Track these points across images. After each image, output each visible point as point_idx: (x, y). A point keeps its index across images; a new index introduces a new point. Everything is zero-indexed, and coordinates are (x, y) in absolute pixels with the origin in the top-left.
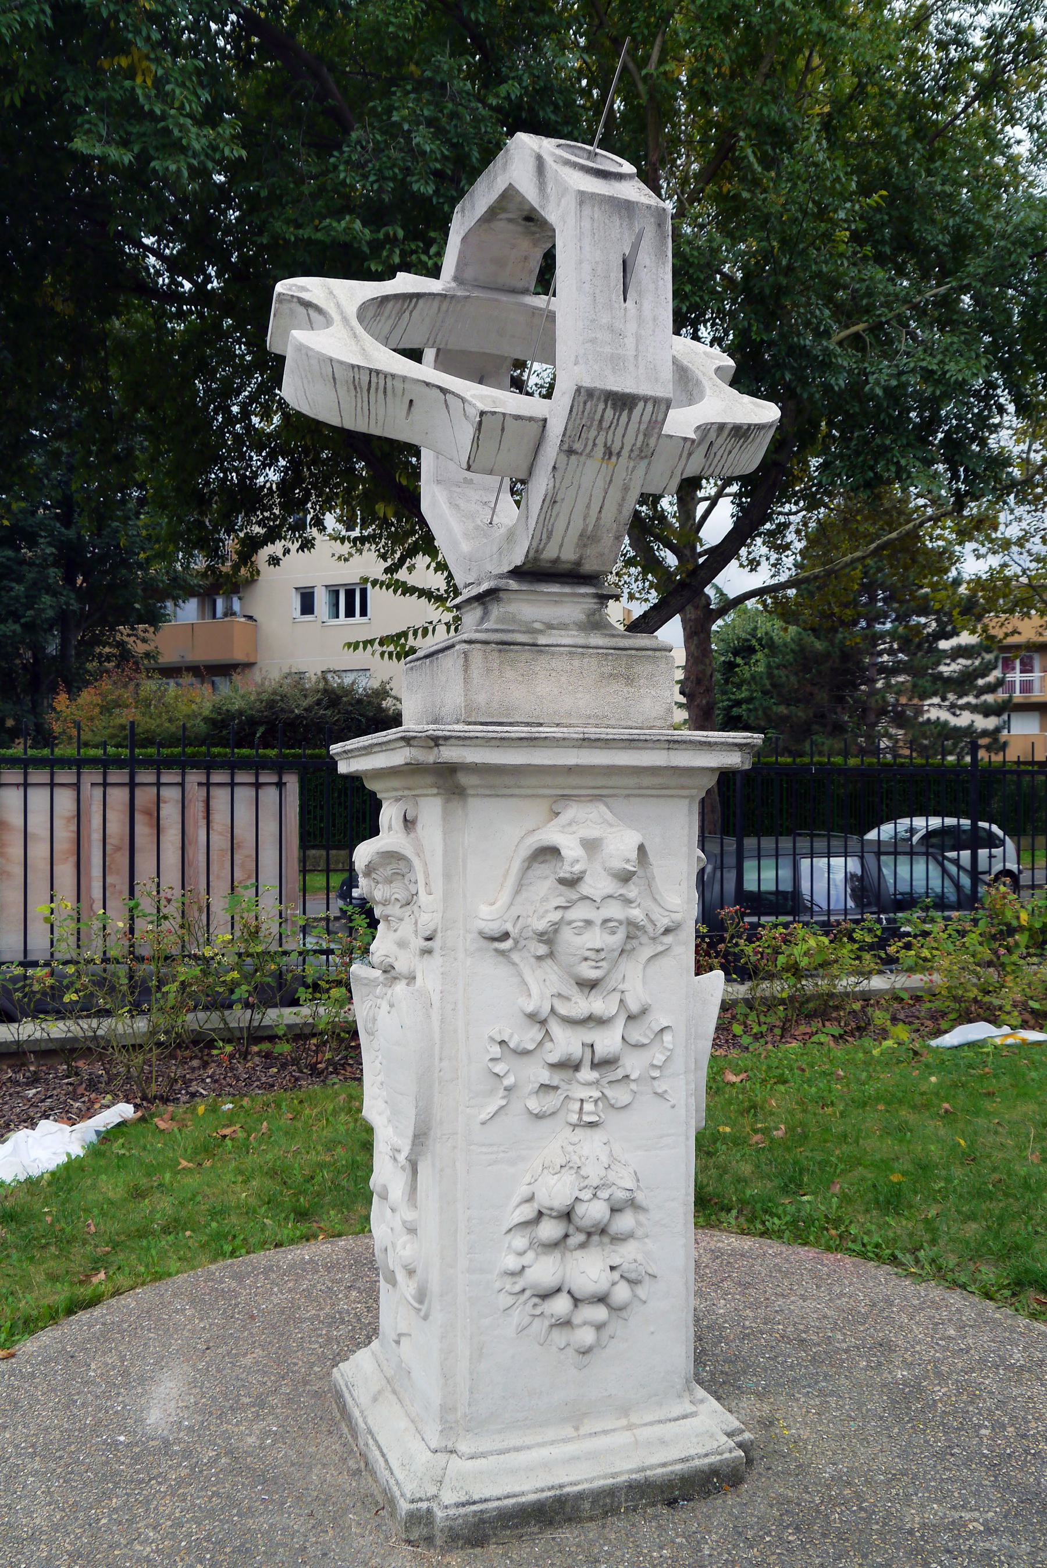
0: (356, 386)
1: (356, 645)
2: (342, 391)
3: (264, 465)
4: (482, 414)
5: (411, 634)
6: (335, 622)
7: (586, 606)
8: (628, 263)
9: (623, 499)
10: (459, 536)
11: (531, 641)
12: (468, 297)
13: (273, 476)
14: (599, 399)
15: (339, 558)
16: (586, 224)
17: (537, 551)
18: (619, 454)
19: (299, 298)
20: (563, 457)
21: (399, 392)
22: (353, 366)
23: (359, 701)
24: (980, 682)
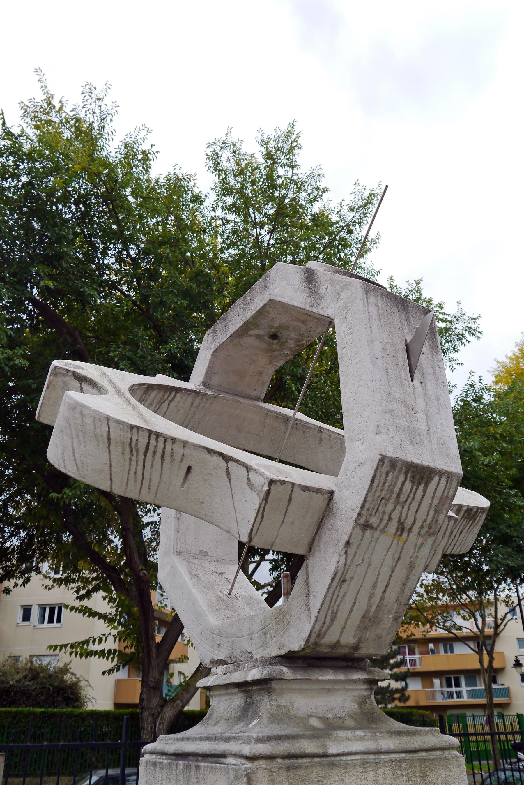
0: (132, 448)
1: (55, 648)
2: (116, 453)
3: (12, 535)
4: (272, 482)
5: (91, 641)
6: (42, 626)
7: (356, 693)
8: (411, 348)
9: (407, 578)
10: (204, 607)
11: (320, 751)
12: (215, 397)
13: (16, 542)
14: (400, 471)
15: (46, 587)
16: (373, 310)
17: (318, 635)
18: (410, 530)
19: (74, 373)
20: (358, 531)
21: (178, 458)
22: (132, 427)
23: (50, 676)
24: (392, 661)
